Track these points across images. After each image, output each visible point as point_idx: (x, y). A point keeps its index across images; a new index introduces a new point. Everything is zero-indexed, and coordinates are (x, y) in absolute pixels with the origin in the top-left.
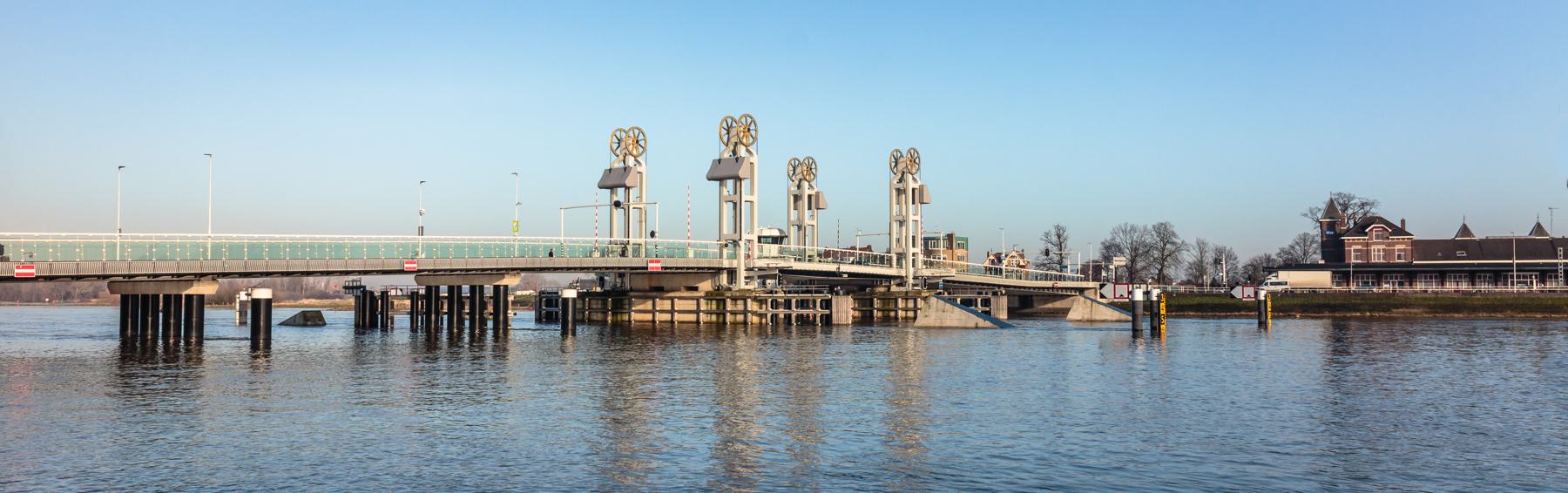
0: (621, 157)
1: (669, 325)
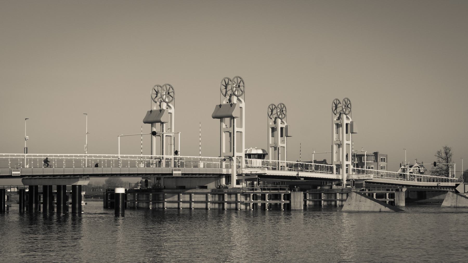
0: (158, 103)
1: (162, 210)
